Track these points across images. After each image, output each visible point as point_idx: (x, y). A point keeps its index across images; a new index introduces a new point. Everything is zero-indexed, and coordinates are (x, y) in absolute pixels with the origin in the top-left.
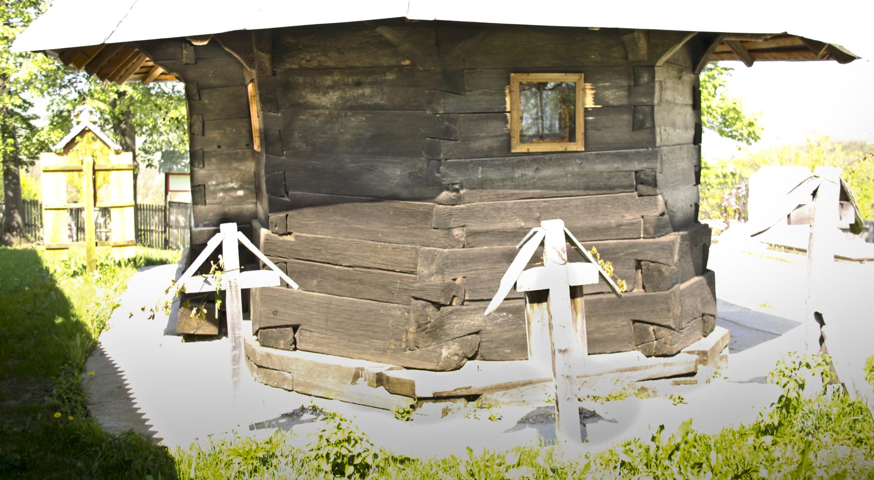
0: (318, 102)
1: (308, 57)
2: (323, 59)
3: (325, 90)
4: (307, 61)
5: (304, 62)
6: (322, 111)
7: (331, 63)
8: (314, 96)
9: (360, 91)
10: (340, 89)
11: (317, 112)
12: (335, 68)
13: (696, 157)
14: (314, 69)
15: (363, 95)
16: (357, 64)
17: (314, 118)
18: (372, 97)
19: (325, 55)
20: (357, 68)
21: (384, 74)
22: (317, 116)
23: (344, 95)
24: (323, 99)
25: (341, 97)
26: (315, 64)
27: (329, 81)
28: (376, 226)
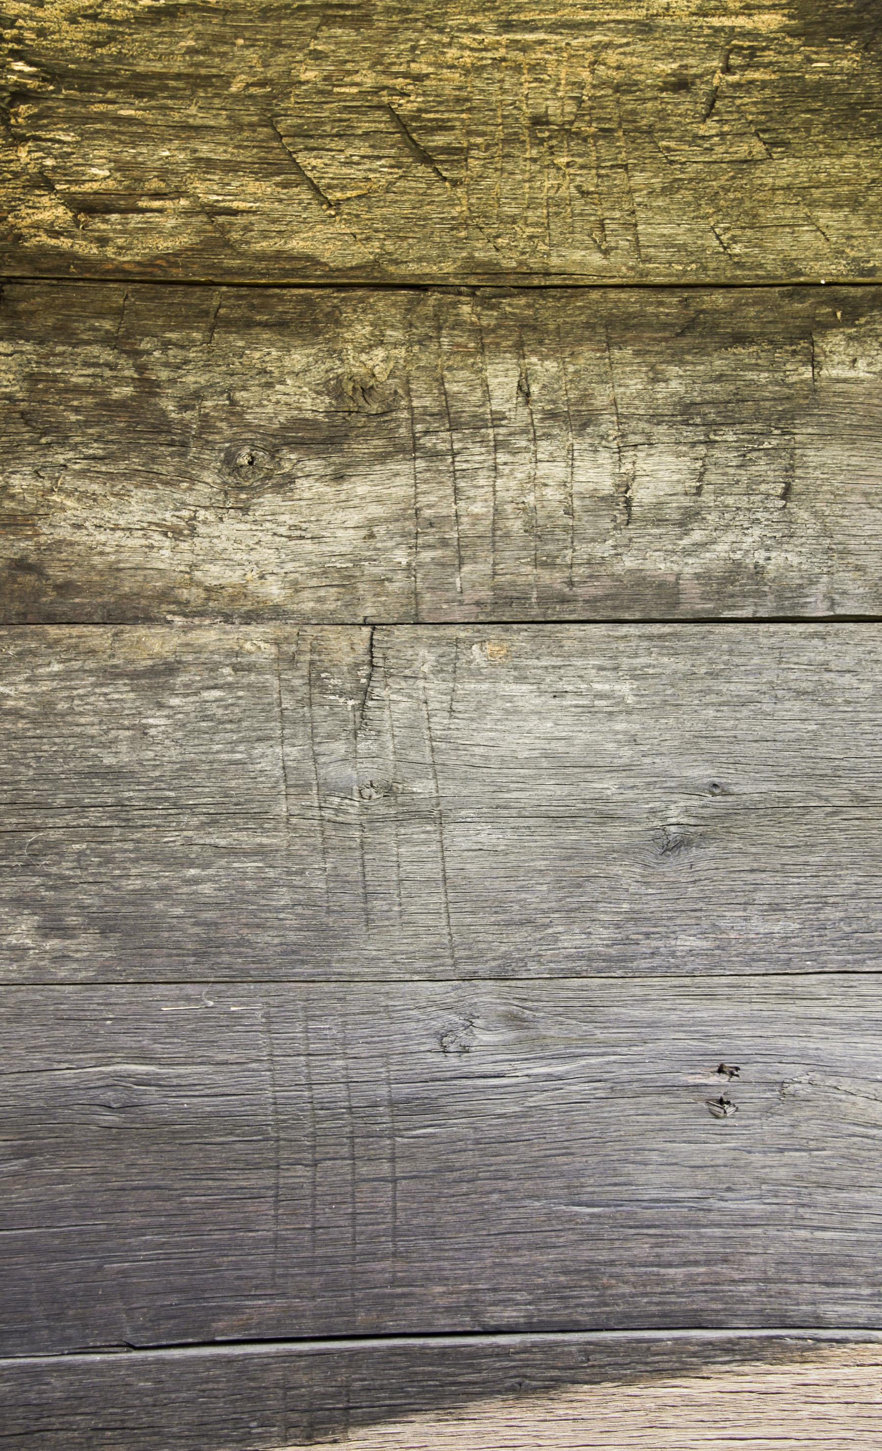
0: (166, 556)
1: (99, 176)
2: (251, 192)
3: (255, 465)
4: (88, 207)
5: (51, 211)
6: (209, 636)
7: (325, 242)
8: (139, 505)
9: (596, 474)
10: (412, 449)
11: (155, 642)
12: (373, 281)
13: (689, 617)
14: (154, 280)
15: (620, 501)
16: (581, 258)
17: (122, 693)
18: (689, 518)
19: (281, 167)
20: (572, 288)
21: (804, 336)
22: (159, 675)
23: (435, 500)
24: (226, 531)
25: (415, 524)
26: (165, 231)
27: (291, 380)
28: (493, 1323)
